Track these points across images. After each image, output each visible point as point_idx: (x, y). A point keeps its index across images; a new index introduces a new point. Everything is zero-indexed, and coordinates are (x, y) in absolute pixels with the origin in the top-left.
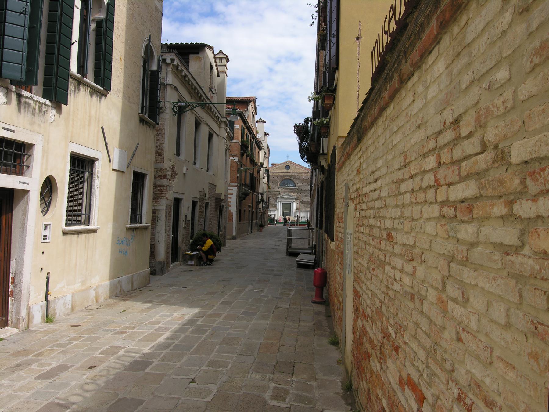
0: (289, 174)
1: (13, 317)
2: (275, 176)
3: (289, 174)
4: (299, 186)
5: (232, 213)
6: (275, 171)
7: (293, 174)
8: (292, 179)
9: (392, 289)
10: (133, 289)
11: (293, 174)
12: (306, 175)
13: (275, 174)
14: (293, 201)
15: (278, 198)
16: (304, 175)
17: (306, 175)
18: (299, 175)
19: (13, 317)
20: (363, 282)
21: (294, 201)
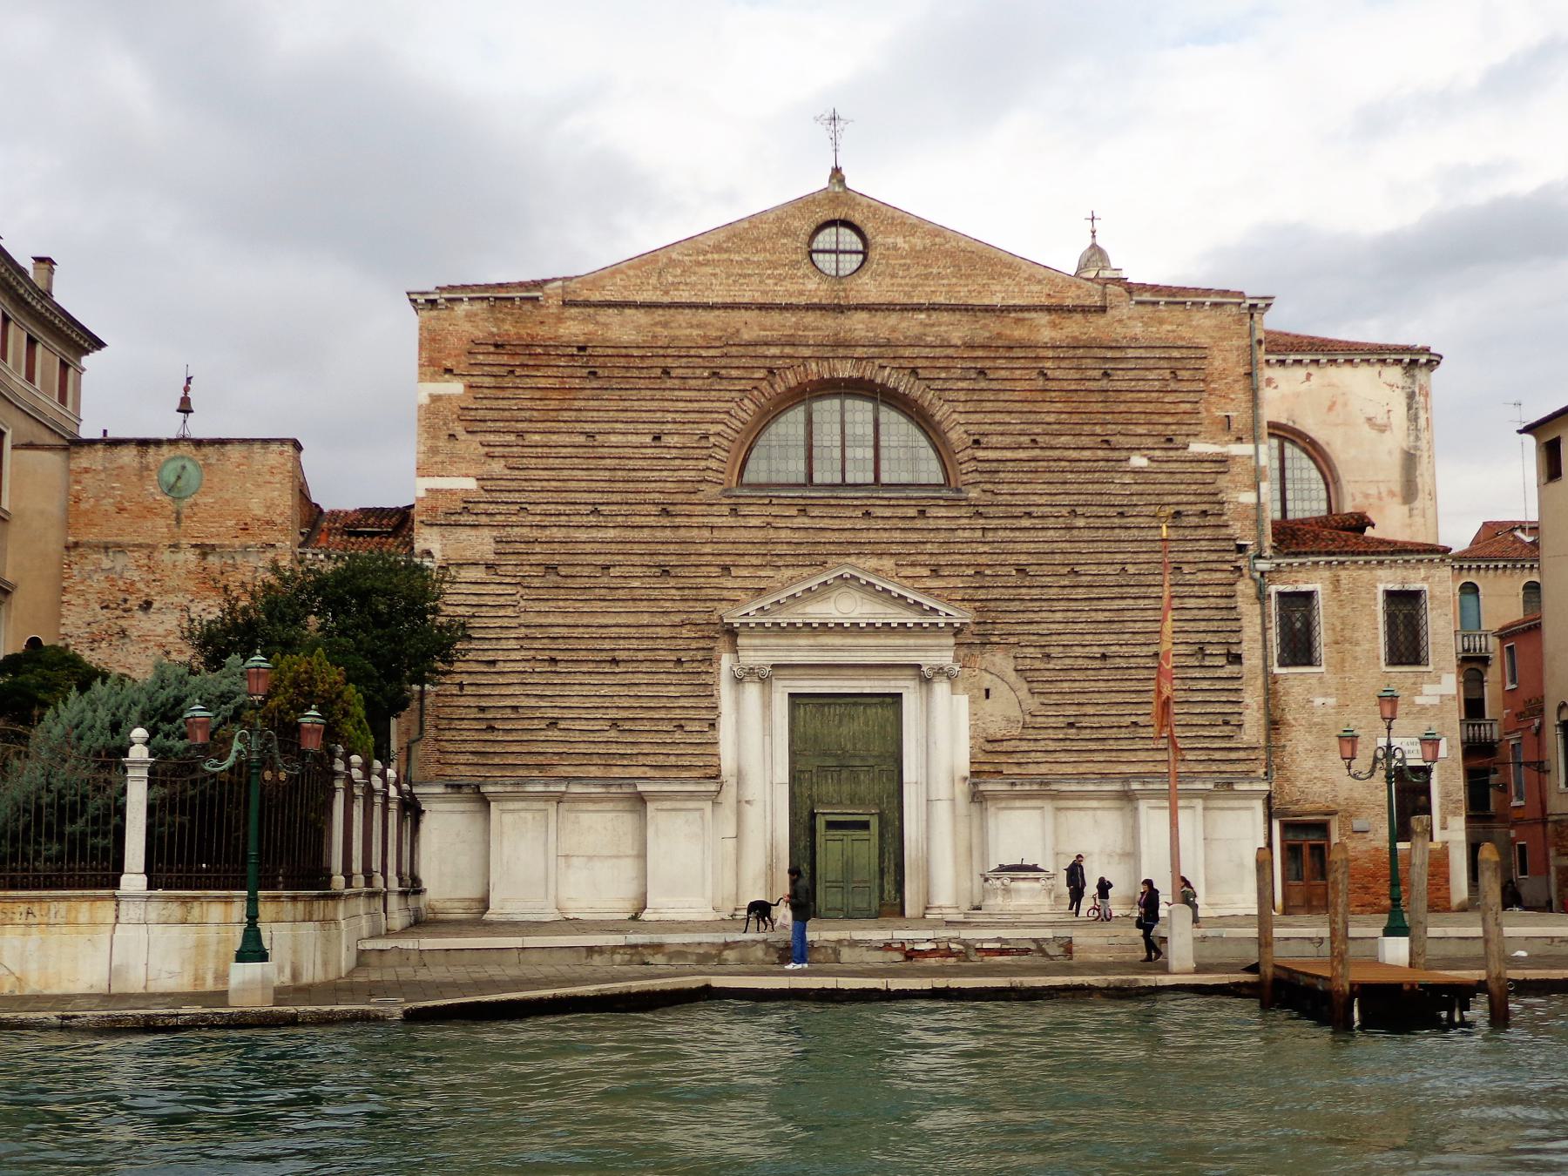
0: (858, 325)
1: (1101, 275)
2: (685, 352)
3: (858, 325)
4: (992, 472)
5: (431, 491)
6: (684, 296)
7: (910, 325)
8: (902, 383)
9: (393, 967)
10: (860, 247)
11: (910, 325)
12: (1074, 328)
13: (684, 327)
14: (928, 660)
15: (732, 633)
16: (1045, 330)
17: (1074, 328)
18: (986, 329)
19: (1101, 275)
20: (793, 1150)
21: (946, 658)
